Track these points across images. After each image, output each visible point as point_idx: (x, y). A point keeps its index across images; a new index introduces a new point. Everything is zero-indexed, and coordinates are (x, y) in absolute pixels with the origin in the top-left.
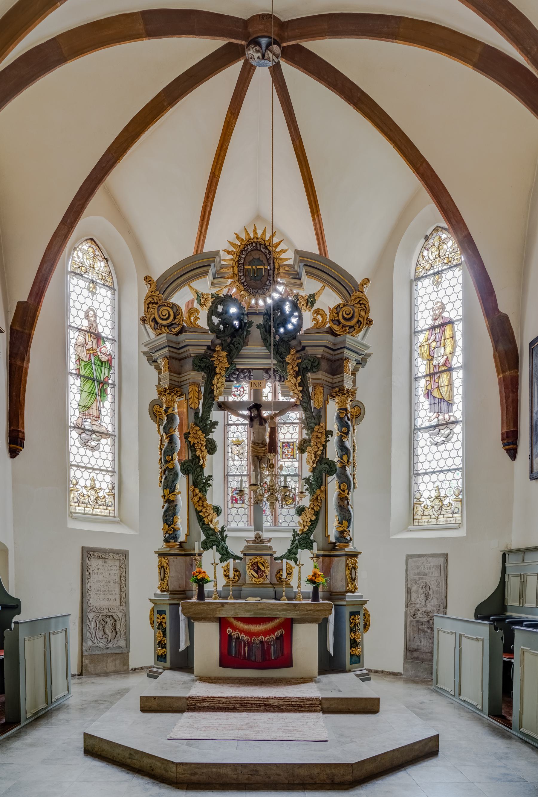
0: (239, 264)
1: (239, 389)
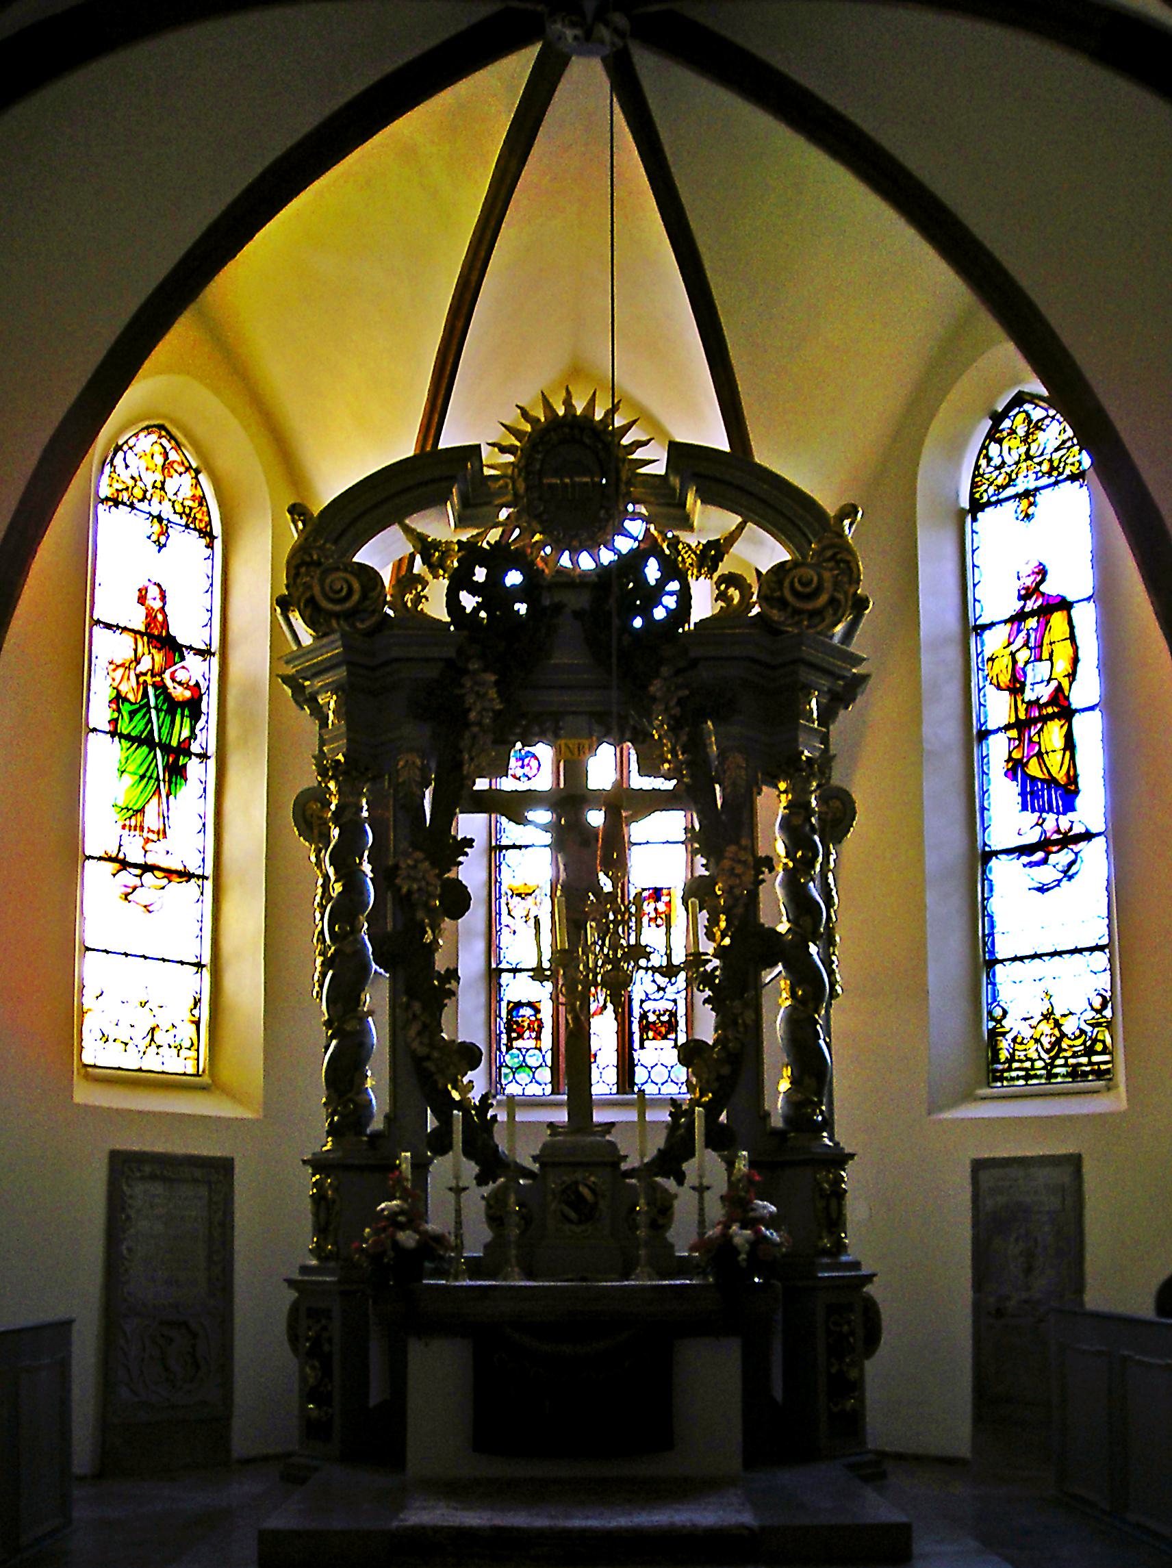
0: (528, 473)
1: (526, 761)
